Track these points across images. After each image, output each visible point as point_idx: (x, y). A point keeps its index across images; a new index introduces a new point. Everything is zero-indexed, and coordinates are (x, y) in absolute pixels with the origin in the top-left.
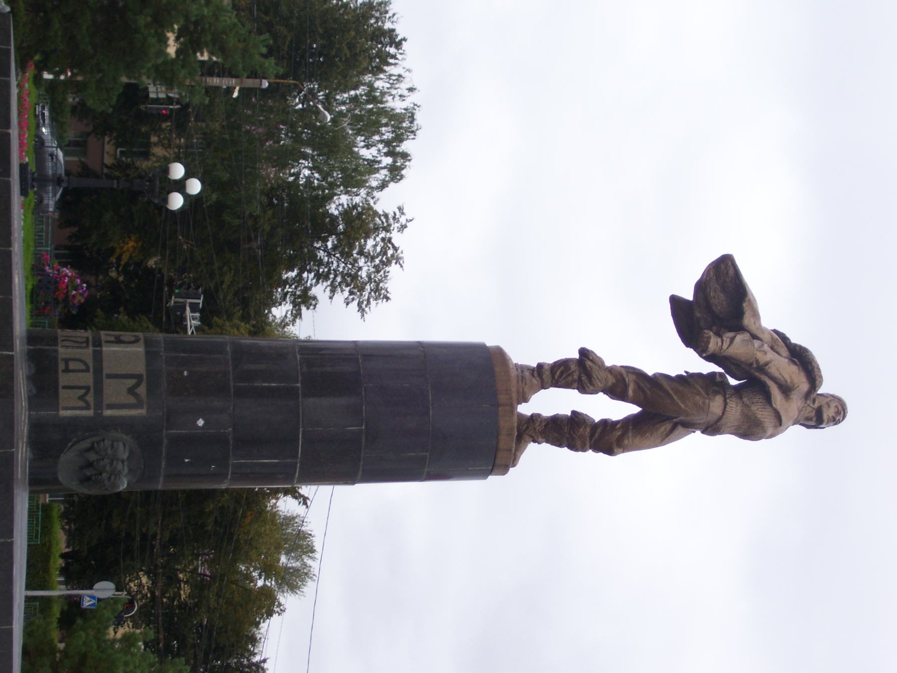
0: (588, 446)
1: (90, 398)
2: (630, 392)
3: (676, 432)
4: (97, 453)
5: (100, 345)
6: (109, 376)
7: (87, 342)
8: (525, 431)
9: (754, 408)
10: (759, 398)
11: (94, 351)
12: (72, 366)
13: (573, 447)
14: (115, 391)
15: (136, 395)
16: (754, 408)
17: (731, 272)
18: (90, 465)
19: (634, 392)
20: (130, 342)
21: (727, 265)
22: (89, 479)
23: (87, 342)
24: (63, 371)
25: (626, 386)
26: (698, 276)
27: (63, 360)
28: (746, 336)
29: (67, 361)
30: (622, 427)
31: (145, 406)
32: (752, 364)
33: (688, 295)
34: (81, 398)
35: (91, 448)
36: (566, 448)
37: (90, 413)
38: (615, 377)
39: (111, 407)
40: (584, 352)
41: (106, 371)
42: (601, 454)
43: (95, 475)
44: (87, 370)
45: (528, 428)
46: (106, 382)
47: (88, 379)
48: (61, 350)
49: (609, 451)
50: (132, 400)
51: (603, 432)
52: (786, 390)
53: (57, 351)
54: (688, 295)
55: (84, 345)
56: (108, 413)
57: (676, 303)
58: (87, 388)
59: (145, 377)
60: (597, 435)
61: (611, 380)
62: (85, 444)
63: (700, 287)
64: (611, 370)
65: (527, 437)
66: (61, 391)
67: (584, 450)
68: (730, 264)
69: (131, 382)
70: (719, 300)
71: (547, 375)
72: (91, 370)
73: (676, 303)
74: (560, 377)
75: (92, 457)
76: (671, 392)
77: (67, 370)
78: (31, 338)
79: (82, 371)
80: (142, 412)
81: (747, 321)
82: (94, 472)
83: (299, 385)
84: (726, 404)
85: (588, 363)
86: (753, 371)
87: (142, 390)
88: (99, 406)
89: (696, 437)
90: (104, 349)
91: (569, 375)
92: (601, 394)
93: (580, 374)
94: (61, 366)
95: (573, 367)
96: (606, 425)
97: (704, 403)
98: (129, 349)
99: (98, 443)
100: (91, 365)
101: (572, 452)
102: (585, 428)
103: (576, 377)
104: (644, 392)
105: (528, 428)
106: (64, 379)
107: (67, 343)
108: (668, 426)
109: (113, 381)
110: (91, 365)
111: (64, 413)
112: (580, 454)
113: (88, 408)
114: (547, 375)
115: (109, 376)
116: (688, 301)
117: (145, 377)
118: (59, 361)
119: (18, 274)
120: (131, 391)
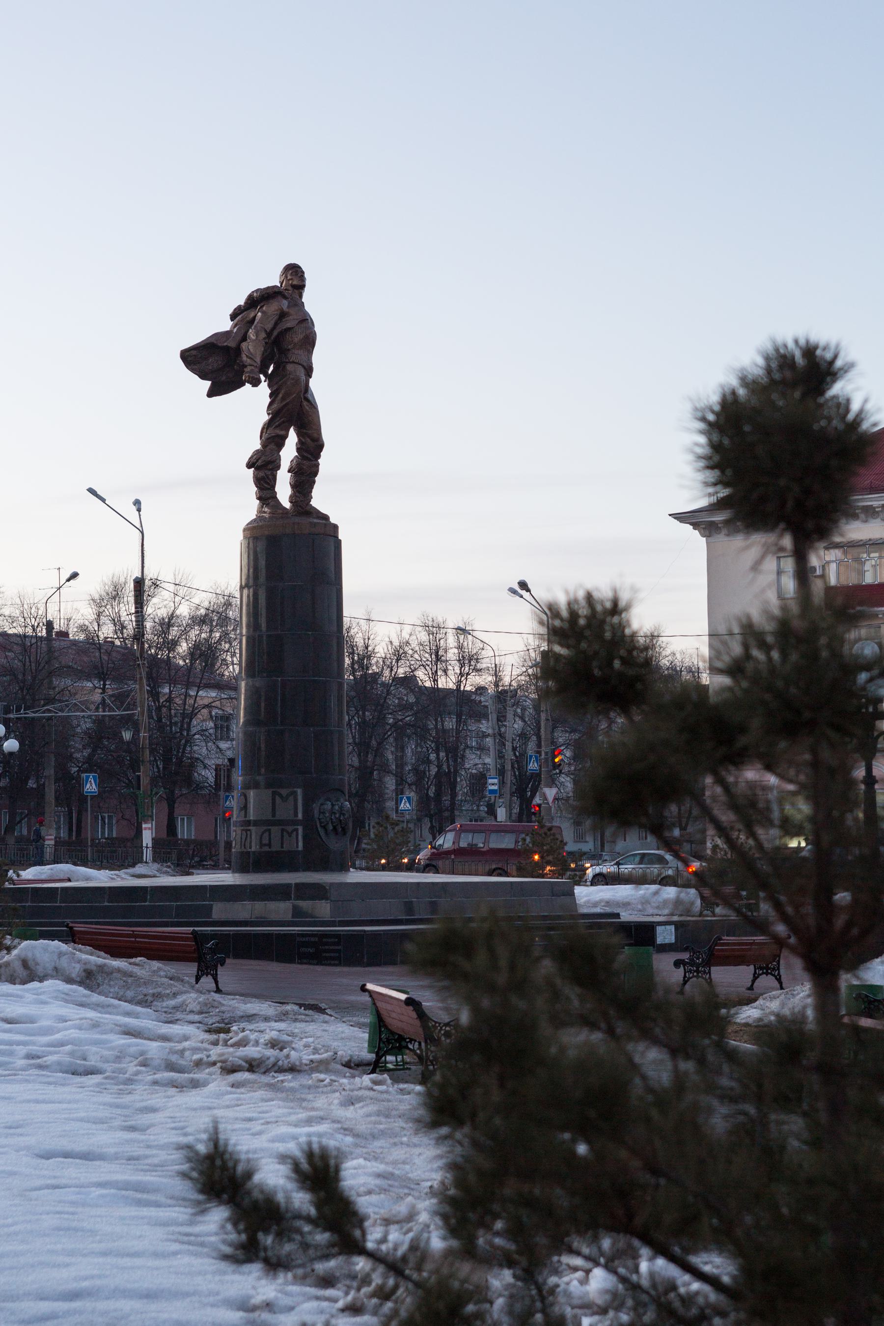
0: (315, 462)
1: (290, 828)
2: (282, 433)
3: (310, 398)
4: (328, 824)
5: (249, 821)
6: (274, 815)
7: (246, 831)
8: (303, 508)
9: (296, 340)
10: (288, 337)
11: (254, 826)
12: (265, 841)
13: (316, 473)
14: (284, 812)
15: (288, 796)
16: (296, 340)
17: (194, 352)
18: (335, 828)
19: (282, 430)
20: (246, 800)
21: (188, 356)
22: (343, 829)
23: (246, 831)
24: (270, 848)
25: (278, 436)
26: (196, 377)
27: (261, 847)
28: (244, 345)
29: (262, 845)
30: (303, 437)
31: (295, 789)
32: (266, 343)
33: (208, 384)
34: (290, 835)
35: (324, 828)
36: (316, 479)
37: (300, 829)
38: (270, 443)
39: (296, 815)
40: (249, 466)
41: (270, 818)
42: (322, 454)
43: (341, 824)
44: (269, 830)
45: (300, 506)
46: (277, 817)
47: (275, 830)
48: (253, 849)
49: (320, 447)
50: (291, 798)
51: (307, 451)
52: (282, 315)
53: (254, 852)
54: (208, 384)
55: (249, 832)
56: (300, 816)
57: (211, 393)
58: (283, 830)
59: (274, 790)
60: (309, 456)
61: (272, 446)
62: (322, 832)
63: (203, 376)
64: (264, 445)
65: (308, 508)
66: (285, 849)
67: (317, 465)
68: (188, 353)
69: (278, 800)
70: (214, 362)
71: (266, 494)
72: (270, 827)
73: (211, 393)
74: (268, 484)
75: (330, 827)
76: (284, 403)
77: (269, 845)
78: (243, 869)
79: (270, 835)
80: (299, 791)
81: (232, 344)
82: (330, 824)
83: (279, 679)
84: (293, 362)
85: (259, 463)
86: (270, 341)
87: (284, 792)
88: (295, 822)
89: (313, 383)
90: (252, 818)
91: (268, 478)
92: (281, 453)
93: (267, 469)
94: (266, 849)
95: (261, 474)
96: (301, 448)
97: (293, 379)
98: (252, 801)
99: (321, 823)
100: (265, 828)
101: (319, 473)
102: (303, 464)
103: (269, 473)
104: (283, 422)
105: (300, 506)
106: (276, 847)
107: (248, 845)
108: (305, 403)
109: (277, 813)
110: (265, 828)
111: (301, 847)
112: (321, 468)
113: (297, 830)
114: (266, 494)
115: (274, 815)
116: (212, 384)
117: (274, 790)
118: (262, 850)
119: (645, 902)
120: (284, 799)
